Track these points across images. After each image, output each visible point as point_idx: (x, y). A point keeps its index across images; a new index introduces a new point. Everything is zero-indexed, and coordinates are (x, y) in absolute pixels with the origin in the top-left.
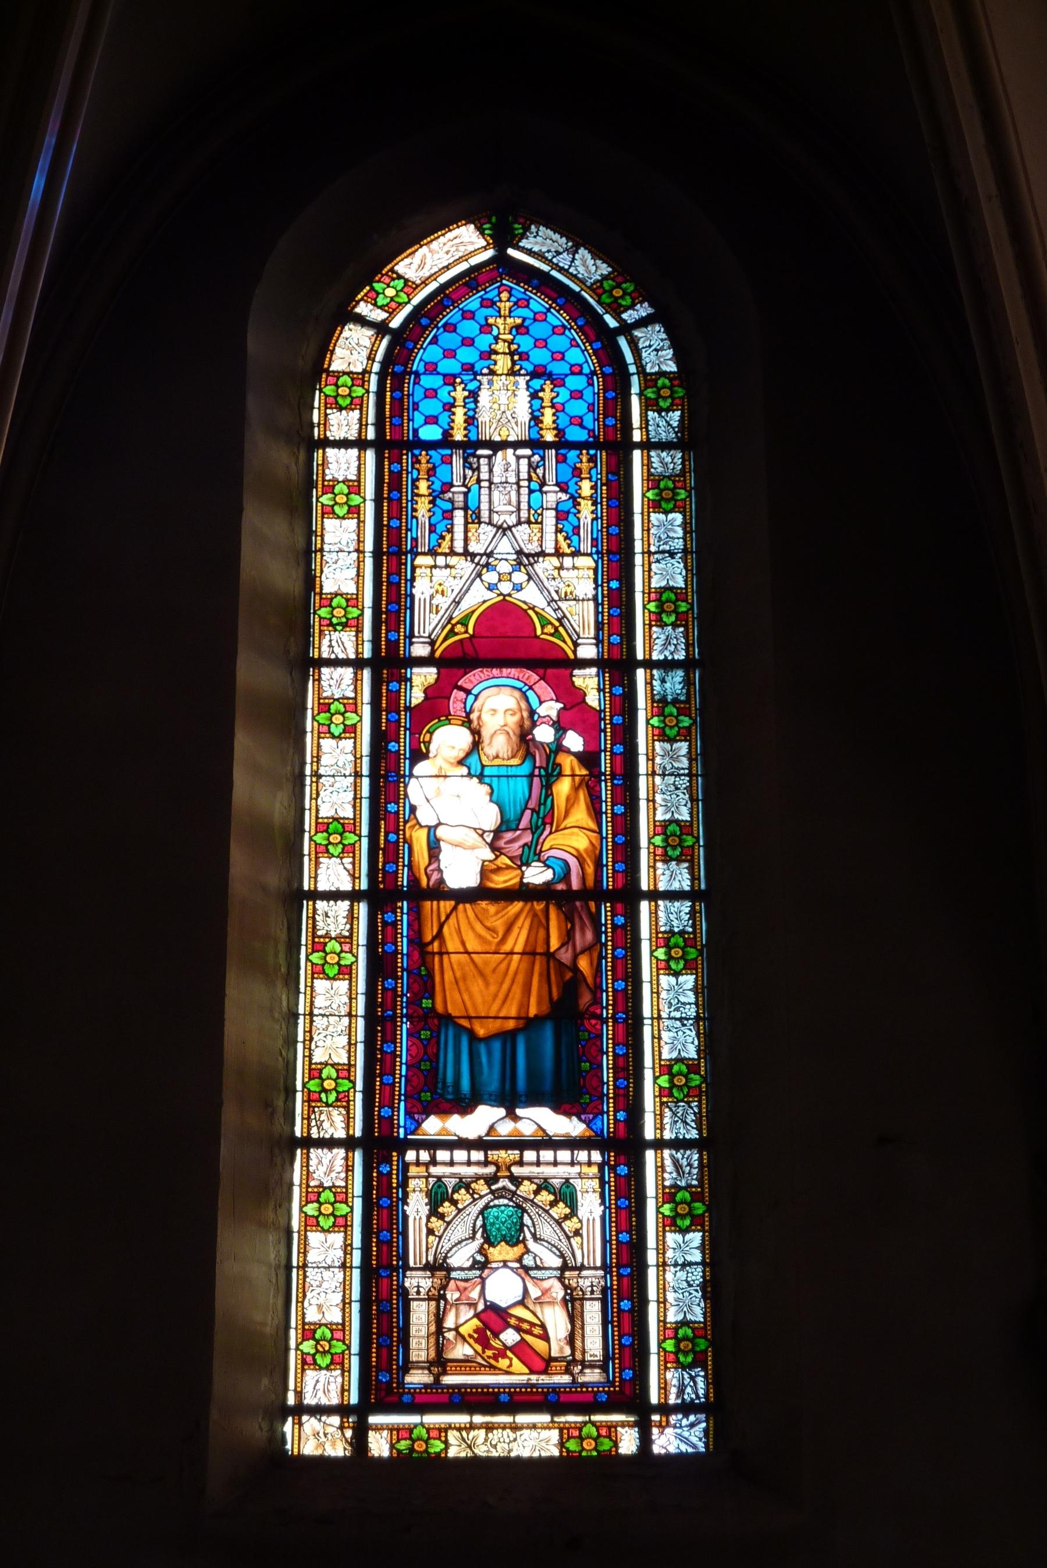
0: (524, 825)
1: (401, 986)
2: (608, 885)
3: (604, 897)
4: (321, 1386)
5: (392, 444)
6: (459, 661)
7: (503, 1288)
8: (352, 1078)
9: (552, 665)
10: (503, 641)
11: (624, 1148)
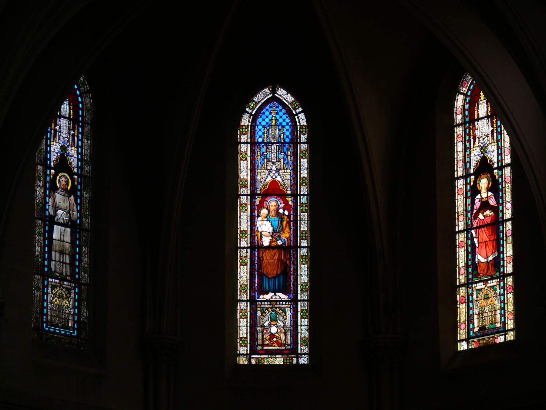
0: (275, 234)
1: (256, 269)
3: (291, 248)
5: (253, 143)
6: (266, 194)
7: (274, 330)
10: (274, 190)
11: (294, 301)
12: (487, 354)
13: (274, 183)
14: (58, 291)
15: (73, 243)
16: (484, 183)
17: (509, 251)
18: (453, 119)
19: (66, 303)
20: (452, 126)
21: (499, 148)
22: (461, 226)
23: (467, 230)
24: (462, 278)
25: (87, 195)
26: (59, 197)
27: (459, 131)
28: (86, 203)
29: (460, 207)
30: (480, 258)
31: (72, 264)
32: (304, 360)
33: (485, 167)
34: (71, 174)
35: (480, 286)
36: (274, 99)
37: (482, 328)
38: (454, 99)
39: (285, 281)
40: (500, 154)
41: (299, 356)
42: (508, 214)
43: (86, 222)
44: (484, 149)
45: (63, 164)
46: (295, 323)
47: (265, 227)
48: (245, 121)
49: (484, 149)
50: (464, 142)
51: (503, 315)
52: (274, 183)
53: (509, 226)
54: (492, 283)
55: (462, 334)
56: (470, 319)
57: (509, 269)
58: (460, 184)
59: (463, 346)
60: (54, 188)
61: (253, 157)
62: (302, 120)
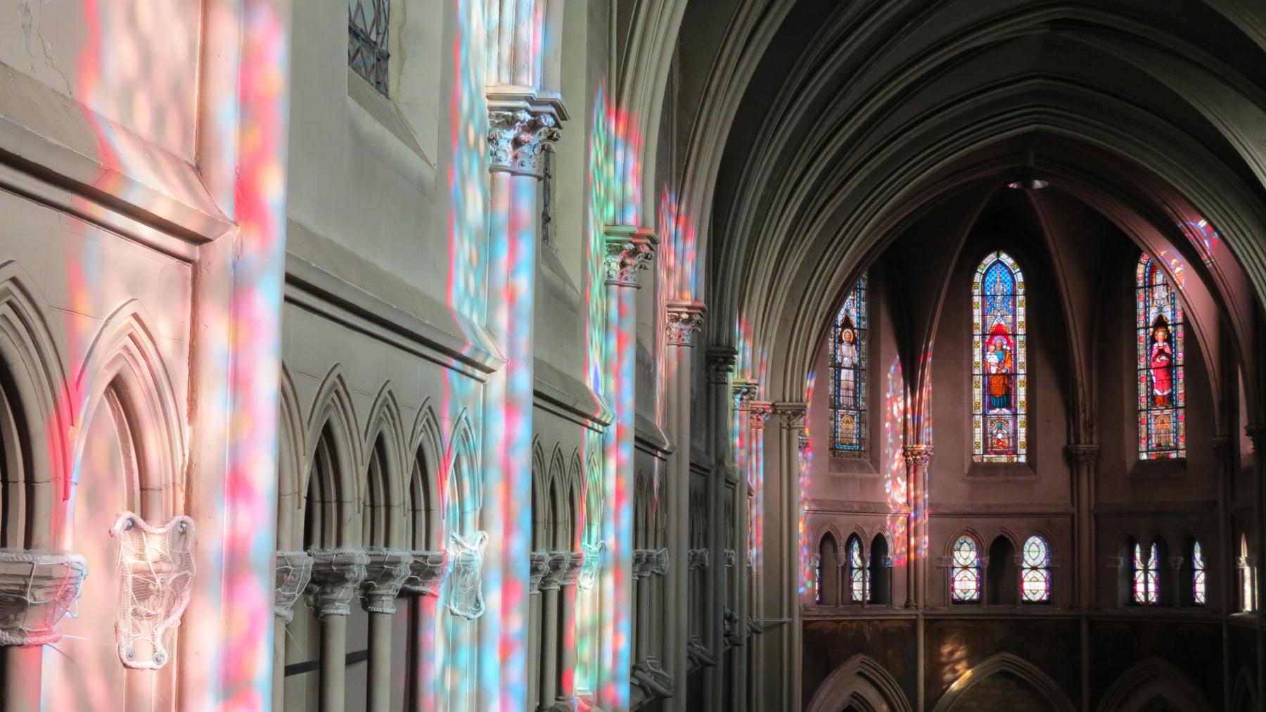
0: (1000, 364)
1: (987, 389)
2: (1146, 593)
3: (1012, 375)
4: (977, 451)
5: (983, 295)
6: (993, 334)
7: (1000, 436)
8: (450, 618)
9: (1005, 335)
10: (999, 331)
11: (1015, 415)
12: (1161, 465)
13: (999, 325)
14: (845, 418)
15: (855, 382)
16: (1160, 335)
17: (1181, 390)
18: (1185, 370)
19: (851, 426)
20: (1134, 287)
21: (1174, 309)
22: (1142, 365)
23: (1148, 369)
24: (1143, 405)
25: (863, 343)
26: (844, 347)
27: (1141, 292)
28: (863, 349)
29: (1142, 352)
30: (1157, 392)
31: (855, 397)
32: (1022, 459)
33: (1160, 323)
34: (853, 329)
35: (1157, 413)
36: (998, 261)
37: (1159, 445)
38: (1135, 268)
39: (1007, 400)
40: (1174, 315)
41: (1018, 455)
42: (1180, 361)
43: (863, 364)
44: (1160, 309)
45: (847, 323)
46: (1015, 432)
47: (993, 359)
48: (978, 278)
49: (1160, 309)
50: (1145, 301)
51: (1176, 438)
52: (999, 325)
53: (1181, 371)
54: (1167, 412)
55: (1143, 447)
56: (1149, 437)
57: (1181, 403)
58: (1141, 333)
59: (1144, 457)
60: (841, 342)
61: (983, 306)
62: (1019, 278)
